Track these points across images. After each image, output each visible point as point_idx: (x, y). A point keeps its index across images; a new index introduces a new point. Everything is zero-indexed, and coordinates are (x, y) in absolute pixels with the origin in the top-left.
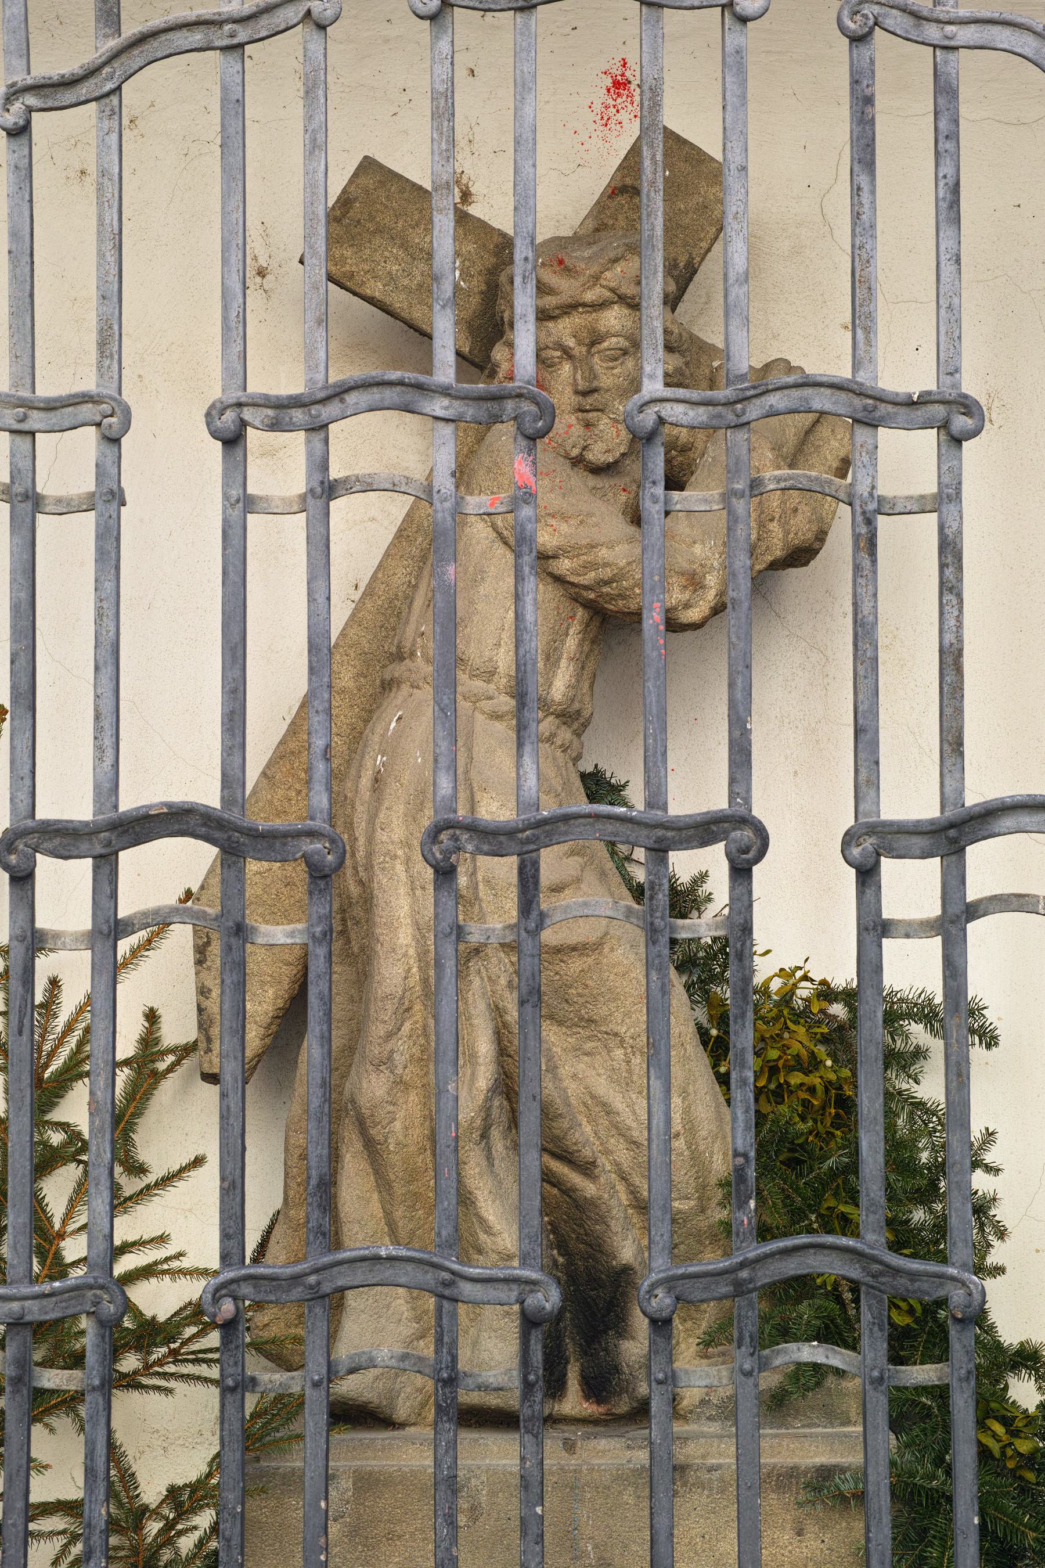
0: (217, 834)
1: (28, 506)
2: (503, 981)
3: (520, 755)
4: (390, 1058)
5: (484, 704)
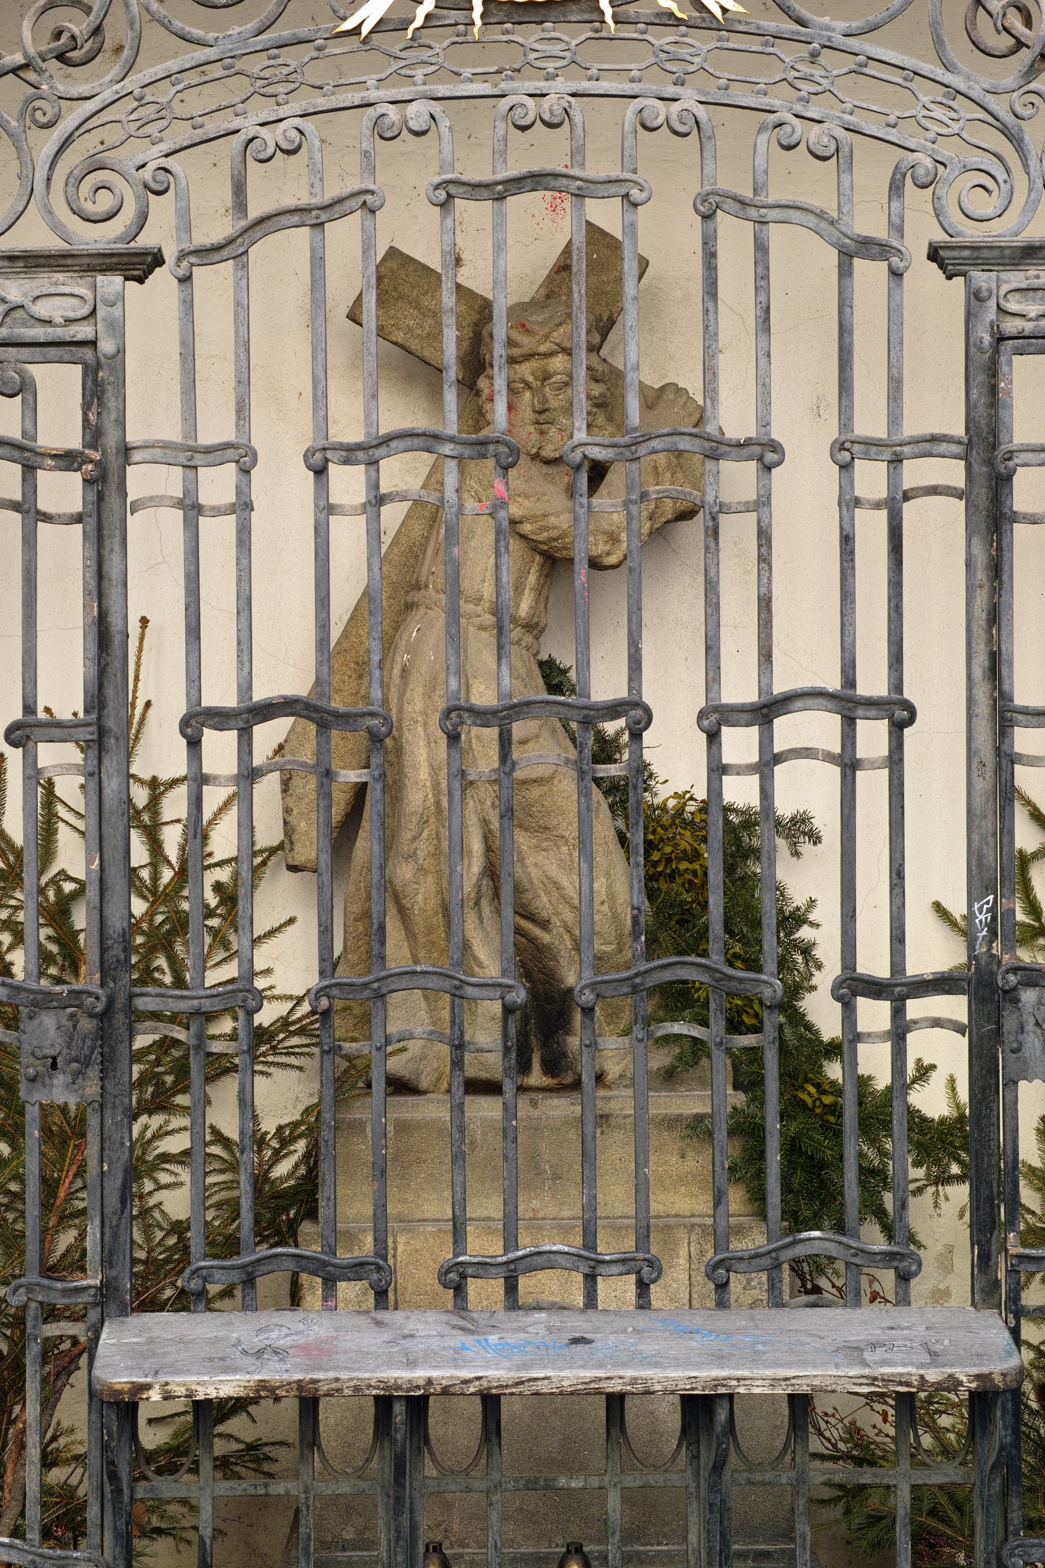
0: (314, 715)
1: (195, 512)
2: (488, 803)
3: (499, 665)
4: (415, 853)
5: (474, 620)
